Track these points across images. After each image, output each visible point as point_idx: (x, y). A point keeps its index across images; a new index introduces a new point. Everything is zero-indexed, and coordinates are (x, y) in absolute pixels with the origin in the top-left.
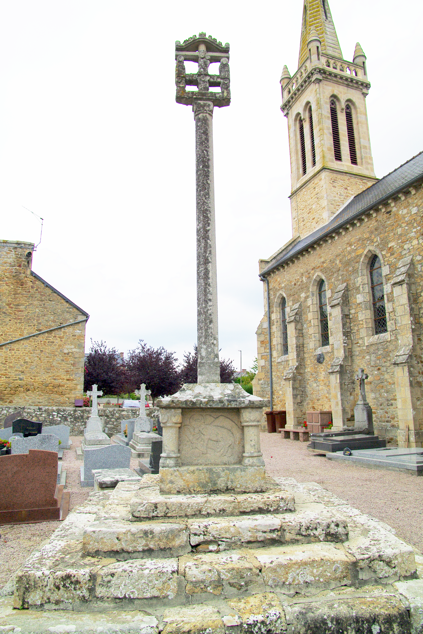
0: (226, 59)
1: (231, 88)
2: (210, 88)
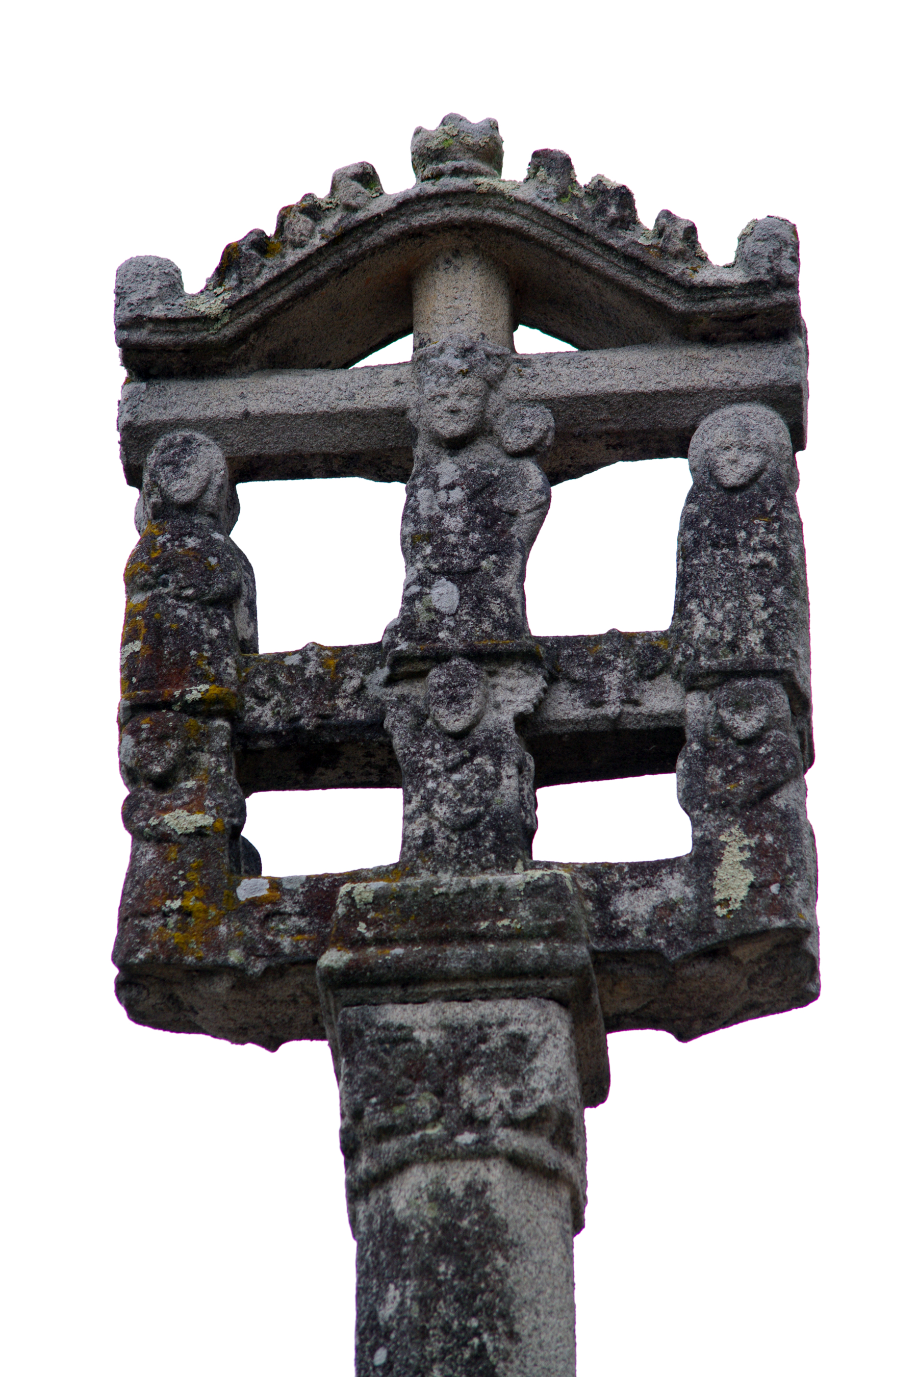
0: (767, 423)
1: (827, 798)
2: (554, 802)
